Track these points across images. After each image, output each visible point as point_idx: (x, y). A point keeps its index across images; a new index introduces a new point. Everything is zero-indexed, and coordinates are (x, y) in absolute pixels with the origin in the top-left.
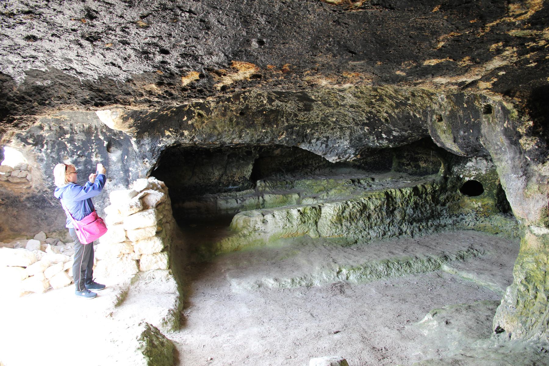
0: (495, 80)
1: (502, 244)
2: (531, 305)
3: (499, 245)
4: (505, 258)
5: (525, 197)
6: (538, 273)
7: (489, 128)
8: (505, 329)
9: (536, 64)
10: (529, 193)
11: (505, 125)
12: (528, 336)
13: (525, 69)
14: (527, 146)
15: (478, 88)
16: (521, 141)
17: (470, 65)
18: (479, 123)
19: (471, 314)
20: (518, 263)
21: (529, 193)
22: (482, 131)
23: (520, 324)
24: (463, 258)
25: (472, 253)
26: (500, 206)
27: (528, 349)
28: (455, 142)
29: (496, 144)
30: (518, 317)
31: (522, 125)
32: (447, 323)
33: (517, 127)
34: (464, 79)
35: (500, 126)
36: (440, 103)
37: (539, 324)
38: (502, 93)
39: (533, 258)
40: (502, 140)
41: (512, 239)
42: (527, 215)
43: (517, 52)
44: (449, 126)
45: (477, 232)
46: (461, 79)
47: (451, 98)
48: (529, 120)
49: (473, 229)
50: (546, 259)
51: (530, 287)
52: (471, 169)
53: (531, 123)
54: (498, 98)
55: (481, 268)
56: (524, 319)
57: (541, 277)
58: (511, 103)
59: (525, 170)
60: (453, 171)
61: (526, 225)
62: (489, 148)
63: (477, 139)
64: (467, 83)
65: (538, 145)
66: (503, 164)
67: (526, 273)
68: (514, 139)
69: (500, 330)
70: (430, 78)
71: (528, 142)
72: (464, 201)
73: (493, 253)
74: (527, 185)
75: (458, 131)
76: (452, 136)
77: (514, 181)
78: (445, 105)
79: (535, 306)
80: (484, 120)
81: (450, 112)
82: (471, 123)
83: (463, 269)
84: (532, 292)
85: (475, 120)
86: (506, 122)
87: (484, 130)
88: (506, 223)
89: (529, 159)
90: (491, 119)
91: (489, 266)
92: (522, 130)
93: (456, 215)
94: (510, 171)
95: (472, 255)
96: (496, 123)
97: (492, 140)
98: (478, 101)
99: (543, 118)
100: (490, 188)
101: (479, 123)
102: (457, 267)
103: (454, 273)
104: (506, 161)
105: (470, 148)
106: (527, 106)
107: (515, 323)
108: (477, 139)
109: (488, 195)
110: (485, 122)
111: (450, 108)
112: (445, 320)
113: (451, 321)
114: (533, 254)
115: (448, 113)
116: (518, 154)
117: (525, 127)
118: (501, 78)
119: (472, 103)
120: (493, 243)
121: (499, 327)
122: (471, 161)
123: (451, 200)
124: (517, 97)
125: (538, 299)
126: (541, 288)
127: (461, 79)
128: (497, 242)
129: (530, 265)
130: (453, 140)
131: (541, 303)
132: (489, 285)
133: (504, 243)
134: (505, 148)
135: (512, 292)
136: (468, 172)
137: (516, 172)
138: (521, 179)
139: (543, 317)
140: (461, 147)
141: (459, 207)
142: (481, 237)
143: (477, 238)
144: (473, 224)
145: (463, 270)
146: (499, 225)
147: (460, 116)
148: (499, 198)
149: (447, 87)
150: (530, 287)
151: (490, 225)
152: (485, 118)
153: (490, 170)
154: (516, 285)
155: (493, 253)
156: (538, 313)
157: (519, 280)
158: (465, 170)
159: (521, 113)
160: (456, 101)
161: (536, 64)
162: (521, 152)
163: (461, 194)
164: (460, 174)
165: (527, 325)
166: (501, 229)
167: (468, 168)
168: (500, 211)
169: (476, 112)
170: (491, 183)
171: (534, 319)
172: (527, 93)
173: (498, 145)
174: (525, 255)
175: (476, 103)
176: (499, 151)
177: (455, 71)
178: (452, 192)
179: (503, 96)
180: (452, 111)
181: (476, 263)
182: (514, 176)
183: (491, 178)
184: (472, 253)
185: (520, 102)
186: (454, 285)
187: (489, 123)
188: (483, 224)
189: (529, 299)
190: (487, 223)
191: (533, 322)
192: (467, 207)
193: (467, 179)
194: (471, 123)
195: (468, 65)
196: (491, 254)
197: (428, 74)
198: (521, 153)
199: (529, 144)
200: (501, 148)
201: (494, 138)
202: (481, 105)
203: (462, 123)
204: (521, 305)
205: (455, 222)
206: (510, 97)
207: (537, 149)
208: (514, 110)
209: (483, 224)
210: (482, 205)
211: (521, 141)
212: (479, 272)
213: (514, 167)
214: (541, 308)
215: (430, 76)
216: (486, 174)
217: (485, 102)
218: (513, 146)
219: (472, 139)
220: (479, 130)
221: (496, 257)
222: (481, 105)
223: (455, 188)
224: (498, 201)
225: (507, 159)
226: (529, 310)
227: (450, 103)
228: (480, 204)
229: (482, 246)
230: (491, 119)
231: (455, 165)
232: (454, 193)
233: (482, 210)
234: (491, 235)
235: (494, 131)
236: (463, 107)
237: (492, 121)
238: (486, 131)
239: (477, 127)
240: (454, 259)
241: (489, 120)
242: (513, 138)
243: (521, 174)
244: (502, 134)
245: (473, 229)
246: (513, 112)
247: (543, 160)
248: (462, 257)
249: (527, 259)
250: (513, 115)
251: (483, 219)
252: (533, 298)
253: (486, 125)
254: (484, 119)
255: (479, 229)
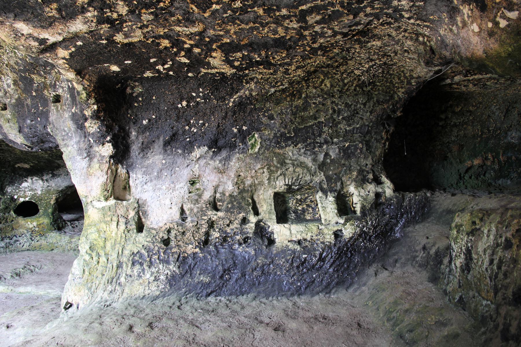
0: (73, 49)
1: (58, 258)
2: (95, 270)
3: (55, 259)
4: (61, 268)
5: (89, 175)
6: (100, 240)
7: (57, 115)
8: (73, 303)
9: (106, 42)
10: (91, 171)
11: (73, 110)
12: (93, 300)
13: (99, 45)
14: (91, 129)
15: (57, 55)
16: (87, 124)
17: (56, 18)
18: (47, 111)
19: (36, 311)
20: (83, 236)
21: (91, 171)
22: (50, 119)
23: (87, 291)
24: (20, 275)
25: (29, 269)
26: (55, 224)
27: (94, 309)
28: (20, 131)
29: (64, 129)
30: (84, 285)
31: (88, 108)
32: (8, 327)
33: (84, 110)
34: (46, 36)
35: (68, 112)
36: (5, 90)
37: (102, 285)
38: (75, 71)
39: (95, 229)
40: (70, 125)
41: (66, 252)
42: (90, 192)
43: (97, 16)
44: (14, 115)
45: (32, 252)
46: (44, 35)
47: (19, 85)
48: (94, 104)
49: (28, 250)
50: (105, 227)
51: (94, 254)
52: (27, 190)
53: (95, 107)
54: (71, 75)
55: (39, 280)
56: (89, 285)
57: (102, 244)
58: (82, 84)
59: (89, 152)
60: (7, 192)
61: (89, 201)
62: (56, 135)
63: (45, 127)
64: (50, 42)
65: (99, 129)
66: (69, 149)
67: (91, 243)
68: (80, 123)
69: (69, 306)
70: (11, 20)
71: (92, 126)
72: (18, 223)
73: (50, 267)
74: (90, 165)
75: (24, 120)
76: (17, 126)
77: (79, 162)
78: (12, 92)
79: (98, 271)
80: (53, 108)
81: (16, 100)
82: (40, 111)
83: (20, 285)
84: (95, 258)
85: (44, 108)
86: (74, 108)
87: (53, 117)
88: (61, 239)
89: (92, 141)
90: (59, 107)
91: (47, 278)
92: (88, 113)
93: (9, 237)
94: (76, 153)
95: (29, 271)
96: (65, 110)
97: (60, 126)
98: (48, 90)
99: (104, 104)
100: (45, 208)
101: (47, 111)
102: (13, 285)
103: (9, 291)
104: (72, 146)
105: (36, 138)
106: (93, 90)
107: (82, 291)
108: (45, 127)
109: (43, 214)
110: (53, 110)
111: (17, 96)
112: (6, 325)
113: (13, 324)
114: (95, 225)
115: (14, 101)
116: (83, 138)
117: (91, 110)
118: (79, 48)
119: (42, 92)
120: (49, 258)
121: (68, 303)
122: (26, 181)
123: (4, 221)
124: (86, 80)
125: (100, 264)
126: (102, 253)
127: (44, 35)
128: (53, 257)
129: (93, 235)
130: (18, 130)
131: (102, 266)
132: (48, 293)
133: (59, 256)
134: (72, 134)
135: (79, 264)
136: (22, 193)
137: (81, 153)
138: (85, 160)
139: (104, 277)
140: (27, 137)
141: (13, 229)
142: (37, 255)
143: (33, 257)
144: (28, 244)
145: (20, 286)
146: (54, 241)
147: (27, 104)
148: (54, 216)
149: (28, 41)
150: (94, 254)
151: (45, 243)
152: (54, 106)
153: (45, 190)
154: (82, 256)
155: (50, 267)
156: (100, 276)
157: (85, 251)
158: (20, 191)
159: (89, 96)
160: (25, 89)
161: (106, 42)
162: (86, 135)
163: (14, 216)
164: (15, 195)
165: (92, 290)
166: (56, 245)
167: (23, 189)
168: (55, 229)
169: (45, 102)
170: (46, 203)
171: (97, 282)
172: (94, 79)
173: (65, 131)
174: (89, 228)
175: (46, 92)
176: (66, 137)
177: (40, 20)
178: (5, 214)
179: (76, 75)
180: (19, 100)
181: (34, 277)
182: (79, 158)
183: (46, 198)
184: (29, 269)
185: (88, 85)
186: (10, 302)
187: (58, 111)
188: (39, 243)
189: (93, 265)
190: (43, 242)
191: (97, 285)
192: (21, 228)
193: (22, 200)
194: (40, 111)
195: (53, 16)
196: (48, 267)
197: (10, 12)
198: (85, 137)
199: (93, 127)
200: (68, 134)
201: (62, 124)
202: (50, 94)
203: (29, 111)
204: (87, 273)
205: (8, 245)
206: (81, 77)
207: (99, 132)
208: (84, 92)
209: (39, 243)
210: (37, 225)
211: (87, 124)
212: (37, 284)
213: (80, 149)
214: (102, 271)
215: (12, 15)
216: (42, 194)
217: (54, 91)
218: (79, 131)
219: (40, 128)
220: (47, 118)
221: (53, 269)
222: (50, 94)
223: (9, 210)
224: (53, 219)
225: (73, 143)
226: (93, 276)
227: (17, 90)
228: (35, 224)
229: (38, 261)
230: (59, 107)
231: (9, 185)
232: (7, 214)
233: (37, 229)
234: (47, 252)
235: (62, 118)
236: (32, 96)
237: (61, 108)
238: (54, 118)
239: (45, 115)
240: (9, 278)
241: (57, 108)
242: (79, 122)
243: (85, 155)
244: (70, 119)
245: (28, 250)
246: (82, 94)
247: (103, 142)
248: (18, 275)
249: (90, 230)
250: (82, 96)
251: (38, 238)
252: (96, 263)
253: (55, 113)
254: (52, 107)
255: (34, 249)
